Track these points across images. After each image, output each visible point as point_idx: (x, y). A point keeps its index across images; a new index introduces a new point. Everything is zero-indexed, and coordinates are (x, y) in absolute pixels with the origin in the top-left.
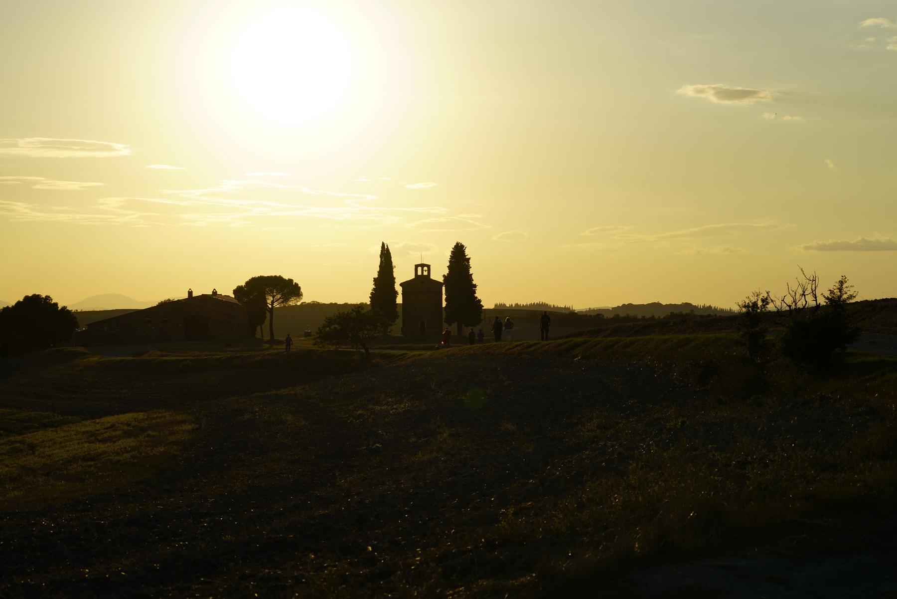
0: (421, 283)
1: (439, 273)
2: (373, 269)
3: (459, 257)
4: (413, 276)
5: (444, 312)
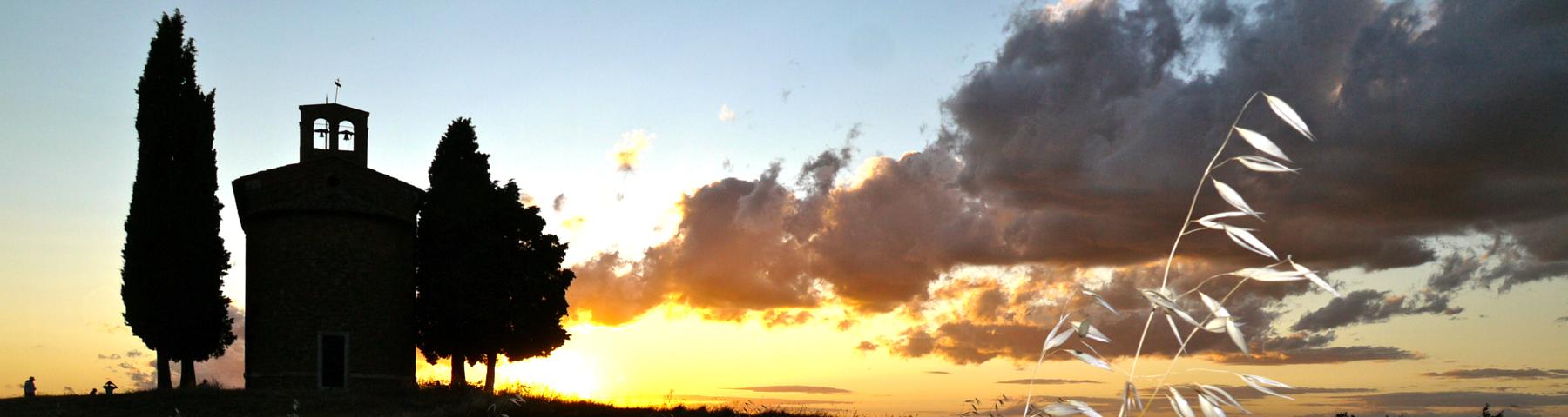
3: (566, 246)
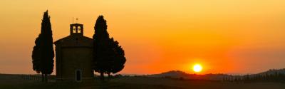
0: (77, 35)
1: (89, 32)
2: (37, 31)
3: (101, 24)
4: (68, 34)
5: (54, 46)
